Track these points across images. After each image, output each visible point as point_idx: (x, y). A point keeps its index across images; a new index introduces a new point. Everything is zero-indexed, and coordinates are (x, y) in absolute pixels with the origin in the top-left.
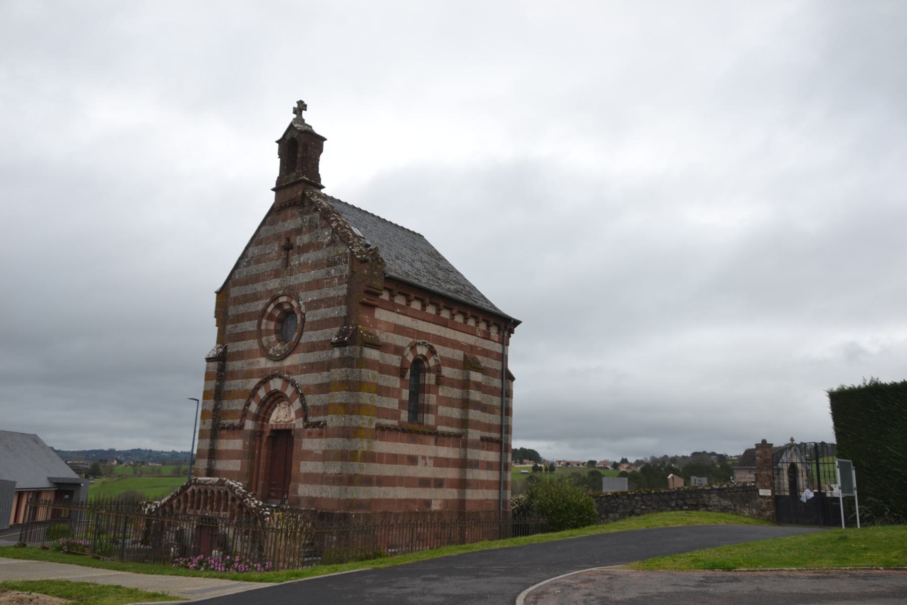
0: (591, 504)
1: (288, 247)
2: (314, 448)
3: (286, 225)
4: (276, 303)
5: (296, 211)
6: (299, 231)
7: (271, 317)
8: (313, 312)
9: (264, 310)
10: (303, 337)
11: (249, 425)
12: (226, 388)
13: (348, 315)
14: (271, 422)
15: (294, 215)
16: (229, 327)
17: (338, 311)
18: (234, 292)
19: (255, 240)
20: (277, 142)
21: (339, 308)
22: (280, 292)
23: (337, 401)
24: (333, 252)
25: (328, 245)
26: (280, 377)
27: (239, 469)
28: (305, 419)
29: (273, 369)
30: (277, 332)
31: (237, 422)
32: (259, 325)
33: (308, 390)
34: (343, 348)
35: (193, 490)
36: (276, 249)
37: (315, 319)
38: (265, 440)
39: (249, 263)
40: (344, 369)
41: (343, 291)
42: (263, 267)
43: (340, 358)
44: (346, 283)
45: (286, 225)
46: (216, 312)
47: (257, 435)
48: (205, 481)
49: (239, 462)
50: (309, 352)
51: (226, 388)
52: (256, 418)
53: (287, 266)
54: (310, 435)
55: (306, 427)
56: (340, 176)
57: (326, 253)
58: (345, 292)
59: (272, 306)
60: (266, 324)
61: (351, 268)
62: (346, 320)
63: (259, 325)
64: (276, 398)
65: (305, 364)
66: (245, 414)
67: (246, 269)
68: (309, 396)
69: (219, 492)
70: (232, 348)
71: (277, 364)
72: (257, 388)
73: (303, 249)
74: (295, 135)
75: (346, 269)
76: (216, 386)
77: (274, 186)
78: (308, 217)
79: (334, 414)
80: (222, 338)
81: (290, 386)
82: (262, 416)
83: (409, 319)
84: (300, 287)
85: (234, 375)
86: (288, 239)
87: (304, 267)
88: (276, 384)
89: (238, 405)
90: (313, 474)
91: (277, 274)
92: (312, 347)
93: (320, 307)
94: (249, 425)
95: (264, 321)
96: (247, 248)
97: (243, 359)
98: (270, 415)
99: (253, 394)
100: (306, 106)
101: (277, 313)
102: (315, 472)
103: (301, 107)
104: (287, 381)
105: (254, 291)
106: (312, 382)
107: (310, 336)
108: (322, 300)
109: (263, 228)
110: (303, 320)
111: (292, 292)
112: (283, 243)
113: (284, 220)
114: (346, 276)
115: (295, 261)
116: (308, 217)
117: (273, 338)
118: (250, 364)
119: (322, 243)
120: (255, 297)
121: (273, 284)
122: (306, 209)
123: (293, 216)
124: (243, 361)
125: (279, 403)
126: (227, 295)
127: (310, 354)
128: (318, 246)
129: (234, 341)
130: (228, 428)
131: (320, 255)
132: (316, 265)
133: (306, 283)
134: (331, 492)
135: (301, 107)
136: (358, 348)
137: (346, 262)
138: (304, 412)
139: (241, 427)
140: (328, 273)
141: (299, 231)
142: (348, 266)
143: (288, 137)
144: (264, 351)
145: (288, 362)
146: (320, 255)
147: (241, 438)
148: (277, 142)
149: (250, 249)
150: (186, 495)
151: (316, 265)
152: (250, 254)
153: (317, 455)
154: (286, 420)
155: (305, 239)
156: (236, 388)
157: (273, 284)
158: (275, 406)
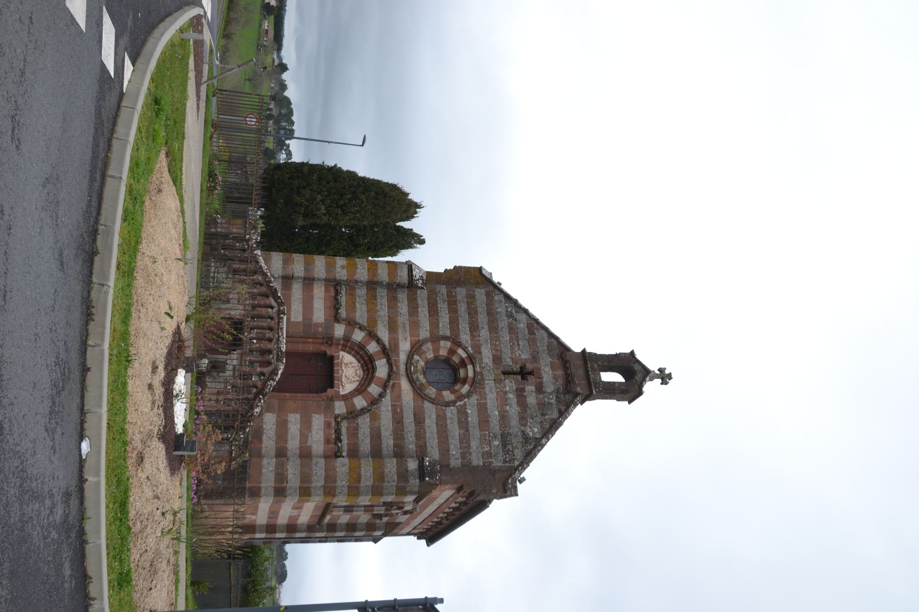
0: (221, 324)
1: (524, 373)
2: (314, 433)
3: (547, 369)
4: (467, 361)
5: (561, 382)
6: (540, 389)
7: (452, 352)
8: (456, 418)
9: (459, 345)
10: (430, 405)
11: (339, 330)
12: (379, 290)
13: (451, 470)
14: (341, 353)
15: (557, 380)
16: (443, 290)
17: (456, 462)
18: (480, 294)
19: (535, 324)
20: (632, 353)
21: (458, 455)
22: (478, 369)
23: (363, 472)
24: (516, 441)
25: (523, 431)
26: (389, 376)
27: (298, 416)
28: (345, 418)
29: (397, 362)
30: (436, 358)
31: (343, 313)
32: (445, 338)
33: (375, 418)
34: (417, 474)
35: (272, 308)
36: (523, 357)
37: (449, 421)
38: (323, 348)
39: (510, 315)
40: (396, 478)
41: (477, 460)
42: (506, 336)
43: (407, 471)
44: (484, 463)
45: (547, 369)
46: (460, 267)
47: (329, 340)
48: (282, 329)
49: (300, 319)
50: (415, 415)
51: (379, 290)
52: (347, 339)
53: (504, 373)
54: (327, 425)
55: (336, 418)
56: (590, 418)
57: (516, 430)
58: (475, 462)
59: (464, 355)
60: (445, 347)
61: (499, 470)
62: (445, 467)
63: (445, 338)
64: (368, 364)
65: (402, 411)
66: (351, 324)
67: (504, 311)
68: (368, 420)
69: (270, 352)
70: (422, 296)
71: (402, 368)
72: (379, 341)
73: (520, 394)
74: (638, 377)
75: (497, 463)
76: (382, 283)
77: (588, 351)
78: (553, 401)
79: (350, 469)
80: (432, 278)
81: (380, 390)
82: (347, 344)
83: (442, 501)
84: (483, 396)
85: (393, 301)
86: (531, 373)
87: (503, 400)
88: (382, 370)
89: (361, 314)
90: (287, 434)
91: (497, 359)
92: (419, 420)
93: (460, 428)
94: (339, 330)
95: (448, 344)
96: (526, 311)
97: (410, 315)
98: (349, 353)
99: (372, 335)
100: (666, 384)
101: (456, 359)
102: (289, 436)
103: (665, 377)
104: (385, 387)
105: (480, 325)
106: (383, 422)
107: (430, 409)
108: (467, 430)
109: (545, 334)
110: (448, 404)
111: (477, 383)
112: (530, 367)
113: (553, 367)
114: (491, 463)
115: (510, 385)
116: (553, 401)
117: (430, 355)
118: (404, 327)
119: (525, 425)
120: (474, 328)
121: (487, 354)
122: (562, 396)
123: (555, 378)
124: (407, 317)
125: (362, 367)
126: (477, 285)
127: (412, 419)
128: (523, 419)
129: (429, 299)
130: (336, 300)
131: (514, 422)
132: (504, 417)
133: (486, 404)
134: (268, 443)
135: (665, 377)
136: (416, 489)
137: (505, 462)
138: (353, 415)
139: (337, 319)
140: (495, 437)
141: (540, 389)
142: (500, 464)
143: (637, 367)
144: (416, 348)
145: (405, 385)
146: (514, 422)
147: (326, 320)
148: (632, 353)
149: (524, 316)
150: (267, 297)
151: (504, 417)
152: (522, 317)
153: (307, 438)
154: (343, 379)
155: (532, 400)
156: (379, 308)
157: (487, 354)
158: (359, 362)
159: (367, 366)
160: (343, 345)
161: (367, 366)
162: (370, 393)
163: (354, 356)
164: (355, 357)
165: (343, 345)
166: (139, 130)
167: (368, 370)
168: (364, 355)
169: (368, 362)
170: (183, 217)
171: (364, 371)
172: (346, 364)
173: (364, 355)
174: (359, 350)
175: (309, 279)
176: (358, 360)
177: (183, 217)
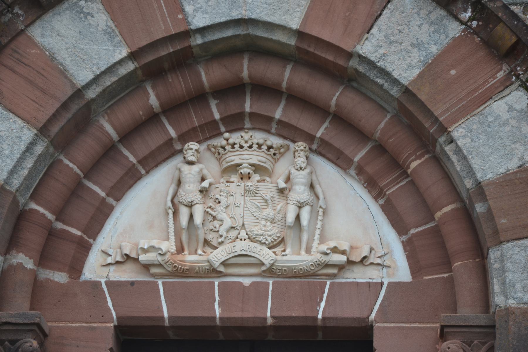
14: (94, 269)
98: (102, 214)
125: (208, 131)
154: (295, 258)
159: (199, 98)
160: (44, 259)
161: (199, 98)
162: (432, 69)
163: (120, 190)
164: (131, 178)
165: (44, 259)
166: (62, 128)
167: (232, 90)
168: (131, 110)
169: (179, 84)
170: (30, 67)
171: (235, 122)
172: (188, 235)
173: (131, 110)
174: (87, 147)
175: (130, 170)
176: (151, 162)
177: (30, 67)
